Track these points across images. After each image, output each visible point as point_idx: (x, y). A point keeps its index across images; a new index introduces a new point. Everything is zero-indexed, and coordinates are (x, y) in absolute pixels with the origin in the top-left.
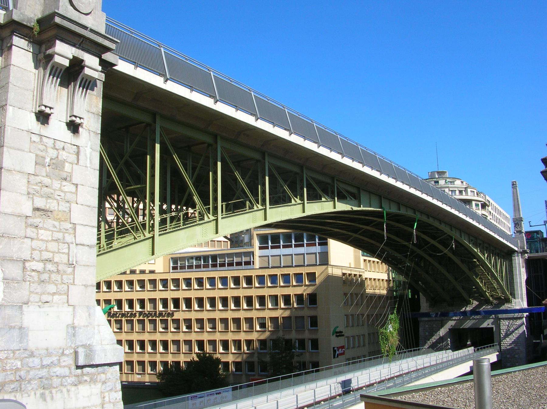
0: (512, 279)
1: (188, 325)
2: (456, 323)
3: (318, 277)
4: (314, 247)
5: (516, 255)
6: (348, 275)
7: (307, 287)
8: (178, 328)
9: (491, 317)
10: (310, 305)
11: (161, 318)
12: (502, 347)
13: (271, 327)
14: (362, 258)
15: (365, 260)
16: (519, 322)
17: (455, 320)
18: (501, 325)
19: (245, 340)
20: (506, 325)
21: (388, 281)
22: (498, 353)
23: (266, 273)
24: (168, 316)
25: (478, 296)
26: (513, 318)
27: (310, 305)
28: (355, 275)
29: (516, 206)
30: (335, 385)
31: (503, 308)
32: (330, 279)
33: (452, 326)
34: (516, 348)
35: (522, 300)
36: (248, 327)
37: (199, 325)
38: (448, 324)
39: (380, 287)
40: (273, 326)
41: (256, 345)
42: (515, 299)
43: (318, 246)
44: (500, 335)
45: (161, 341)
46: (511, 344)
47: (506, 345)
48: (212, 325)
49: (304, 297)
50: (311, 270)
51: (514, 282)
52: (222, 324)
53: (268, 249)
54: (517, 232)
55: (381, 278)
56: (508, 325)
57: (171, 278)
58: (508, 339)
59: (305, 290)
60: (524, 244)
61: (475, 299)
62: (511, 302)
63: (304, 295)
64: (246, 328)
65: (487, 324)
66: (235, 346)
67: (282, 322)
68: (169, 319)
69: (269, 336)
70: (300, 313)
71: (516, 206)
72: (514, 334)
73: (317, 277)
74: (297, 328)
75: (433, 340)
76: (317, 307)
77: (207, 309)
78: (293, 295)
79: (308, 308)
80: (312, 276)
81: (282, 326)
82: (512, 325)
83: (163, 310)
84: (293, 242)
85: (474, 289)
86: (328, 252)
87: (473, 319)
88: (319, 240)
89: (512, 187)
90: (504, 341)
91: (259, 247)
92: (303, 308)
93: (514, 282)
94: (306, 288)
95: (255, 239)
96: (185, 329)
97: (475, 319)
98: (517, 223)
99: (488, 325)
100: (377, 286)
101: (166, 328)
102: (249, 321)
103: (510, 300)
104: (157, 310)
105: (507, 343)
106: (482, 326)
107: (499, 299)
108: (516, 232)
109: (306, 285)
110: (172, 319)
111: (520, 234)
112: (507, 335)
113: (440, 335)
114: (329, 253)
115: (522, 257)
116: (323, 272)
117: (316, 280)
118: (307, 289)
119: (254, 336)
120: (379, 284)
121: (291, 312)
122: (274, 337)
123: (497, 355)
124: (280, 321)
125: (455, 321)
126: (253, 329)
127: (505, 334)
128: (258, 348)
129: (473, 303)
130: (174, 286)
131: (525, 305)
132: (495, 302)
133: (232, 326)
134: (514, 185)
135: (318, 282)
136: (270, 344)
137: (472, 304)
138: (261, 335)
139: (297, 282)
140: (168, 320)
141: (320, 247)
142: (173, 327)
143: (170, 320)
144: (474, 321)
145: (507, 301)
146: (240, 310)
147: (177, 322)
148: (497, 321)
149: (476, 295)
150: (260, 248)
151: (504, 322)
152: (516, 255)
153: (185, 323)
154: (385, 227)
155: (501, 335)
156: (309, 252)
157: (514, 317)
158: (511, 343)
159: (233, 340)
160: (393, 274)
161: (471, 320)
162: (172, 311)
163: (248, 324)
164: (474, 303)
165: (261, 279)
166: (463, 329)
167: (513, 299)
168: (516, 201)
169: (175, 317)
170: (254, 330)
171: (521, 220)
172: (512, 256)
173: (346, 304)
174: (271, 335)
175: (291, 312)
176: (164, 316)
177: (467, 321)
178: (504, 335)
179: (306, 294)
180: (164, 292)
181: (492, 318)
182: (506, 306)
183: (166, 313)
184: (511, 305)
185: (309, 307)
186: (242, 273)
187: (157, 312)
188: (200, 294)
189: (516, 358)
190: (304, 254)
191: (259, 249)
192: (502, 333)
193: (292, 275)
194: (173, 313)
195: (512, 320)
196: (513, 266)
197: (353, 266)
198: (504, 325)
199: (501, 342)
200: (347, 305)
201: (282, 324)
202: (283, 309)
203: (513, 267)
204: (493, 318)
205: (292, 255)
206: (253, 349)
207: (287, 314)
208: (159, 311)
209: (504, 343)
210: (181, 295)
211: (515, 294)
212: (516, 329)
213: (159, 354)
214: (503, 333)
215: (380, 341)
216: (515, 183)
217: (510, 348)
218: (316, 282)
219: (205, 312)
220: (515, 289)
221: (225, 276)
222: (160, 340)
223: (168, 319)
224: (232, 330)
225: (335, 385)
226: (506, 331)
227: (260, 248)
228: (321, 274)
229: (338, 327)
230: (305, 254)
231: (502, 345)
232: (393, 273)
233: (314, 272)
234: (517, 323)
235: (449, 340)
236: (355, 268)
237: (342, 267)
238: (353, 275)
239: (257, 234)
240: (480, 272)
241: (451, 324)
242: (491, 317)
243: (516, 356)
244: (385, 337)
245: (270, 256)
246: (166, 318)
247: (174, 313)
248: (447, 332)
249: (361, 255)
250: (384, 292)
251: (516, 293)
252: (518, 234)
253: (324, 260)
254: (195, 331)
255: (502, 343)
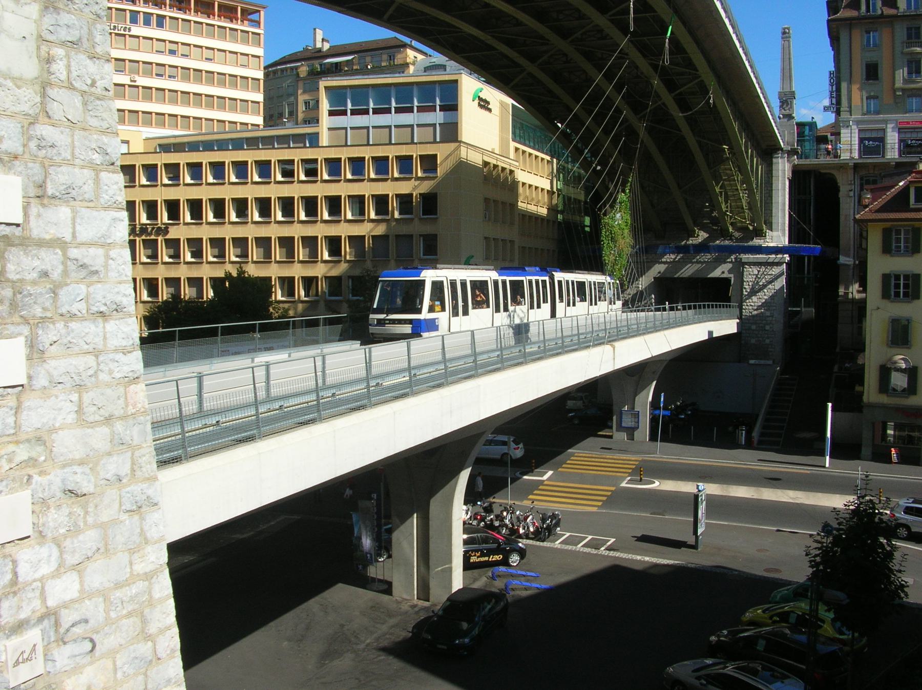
0: (769, 196)
1: (195, 250)
2: (667, 268)
3: (441, 163)
4: (432, 114)
5: (780, 155)
6: (492, 166)
7: (419, 182)
8: (176, 256)
9: (728, 260)
10: (423, 214)
11: (144, 237)
12: (744, 311)
13: (350, 254)
14: (513, 145)
15: (517, 149)
16: (776, 270)
17: (665, 263)
18: (745, 274)
19: (302, 277)
20: (753, 275)
21: (551, 193)
22: (738, 321)
23: (344, 154)
24: (158, 234)
25: (708, 223)
26: (766, 262)
27: (423, 214)
28: (503, 169)
29: (787, 71)
30: (505, 329)
31: (757, 242)
32: (462, 167)
33: (659, 273)
34: (768, 314)
35: (784, 235)
36: (308, 254)
37: (216, 251)
38: (653, 269)
39: (538, 202)
40: (354, 253)
41: (322, 286)
42: (772, 231)
43: (440, 111)
44: (743, 291)
45: (144, 279)
46: (759, 308)
47: (751, 308)
48: (239, 249)
49: (414, 200)
50: (429, 150)
51: (772, 203)
52: (259, 249)
53: (347, 115)
54: (785, 116)
55: (541, 185)
56: (757, 275)
57: (163, 162)
58: (754, 298)
59: (415, 188)
60: (794, 139)
61: (703, 228)
62: (765, 236)
63: (414, 195)
64: (303, 255)
65: (721, 271)
66: (282, 289)
67: (371, 245)
68: (160, 238)
69: (347, 271)
70: (405, 230)
71: (787, 71)
72: (765, 291)
73: (438, 163)
74: (398, 257)
75: (625, 295)
76: (437, 218)
77: (231, 220)
78: (393, 196)
79: (421, 219)
80: (429, 162)
81: (371, 254)
82: (763, 276)
83: (148, 222)
84: (394, 104)
85: (707, 207)
86: (457, 123)
87: (698, 262)
88: (441, 101)
89: (782, 38)
90: (748, 301)
91: (329, 111)
92: (412, 219)
93: (773, 201)
94: (417, 183)
95: (323, 98)
96: (189, 258)
97: (700, 262)
98: (786, 101)
99: (723, 272)
100: (533, 199)
101: (154, 256)
102: (310, 242)
103: (762, 233)
104: (137, 222)
105: (753, 304)
106: (711, 275)
107: (744, 229)
108: (781, 116)
109: (418, 179)
110: (165, 240)
111: (788, 121)
112: (753, 292)
113: (638, 287)
114: (459, 125)
115: (788, 161)
116: (450, 155)
117: (437, 169)
118: (419, 185)
119: (319, 271)
120: (536, 195)
121: (389, 228)
122: (357, 272)
123: (738, 323)
124: (368, 243)
125: (667, 265)
126: (318, 258)
127: (751, 289)
128: (325, 292)
129: (698, 235)
130: (170, 179)
131: (785, 241)
132: (737, 234)
133: (277, 253)
134: (785, 33)
135: (440, 172)
136: (347, 285)
137: (697, 237)
138: (331, 269)
139: (400, 173)
140: (157, 240)
141: (442, 113)
142: (167, 255)
143: (162, 241)
144: (696, 267)
145: (759, 233)
146: (293, 222)
147: (174, 244)
148: (739, 267)
149: (705, 221)
150: (331, 113)
151: (750, 270)
152: (780, 155)
153: (189, 247)
154: (632, 6)
155: (744, 290)
156: (422, 123)
157: (769, 261)
158: (759, 306)
159: (279, 277)
160: (559, 182)
161: (693, 263)
162: (164, 224)
163: (308, 249)
164: (701, 234)
165: (334, 165)
166: (678, 278)
167: (768, 231)
168: (787, 62)
169: (170, 236)
170: (320, 259)
171: (792, 95)
172: (772, 158)
173: (487, 219)
174: (350, 268)
175: (387, 228)
176: (150, 234)
177: (686, 265)
178: (749, 291)
179: (416, 196)
180: (150, 189)
181: (729, 262)
182: (757, 242)
183: (153, 229)
184: (764, 242)
185: (422, 219)
186: (297, 154)
187: (138, 226)
188: (218, 193)
189: (767, 330)
190: (412, 126)
191: (329, 115)
192: (745, 288)
193: (393, 158)
194: (167, 228)
195: (764, 266)
196: (774, 175)
197: (497, 151)
198: (750, 274)
199: (742, 302)
200: (489, 220)
201: (371, 250)
202: (373, 221)
203: (772, 177)
204: (731, 262)
205: (390, 127)
206: (317, 295)
207: (380, 230)
208: (140, 224)
209: (747, 305)
210: (182, 194)
211: (772, 223)
212: (770, 282)
213: (142, 304)
214: (747, 287)
215: (603, 241)
216: (787, 31)
217: (757, 315)
218: (437, 172)
219: (227, 226)
220: (773, 215)
221: (265, 159)
222: (143, 279)
223: (157, 240)
224: (278, 259)
225: (505, 329)
226: (752, 285)
227: (331, 113)
228: (447, 158)
229: (473, 256)
230: (415, 126)
231: (744, 307)
232: (559, 181)
233: (434, 153)
234: (773, 271)
235: (653, 296)
236: (504, 157)
237: (482, 151)
238: (500, 169)
239: (325, 87)
240: (727, 175)
241: (658, 269)
242: (728, 260)
243: (767, 327)
244: (611, 234)
245: (349, 129)
246: (153, 237)
247: (168, 228)
248: (651, 284)
249: (511, 140)
250: (543, 211)
251: (774, 221)
252: (786, 120)
253: (451, 132)
254: (209, 260)
255: (745, 304)
